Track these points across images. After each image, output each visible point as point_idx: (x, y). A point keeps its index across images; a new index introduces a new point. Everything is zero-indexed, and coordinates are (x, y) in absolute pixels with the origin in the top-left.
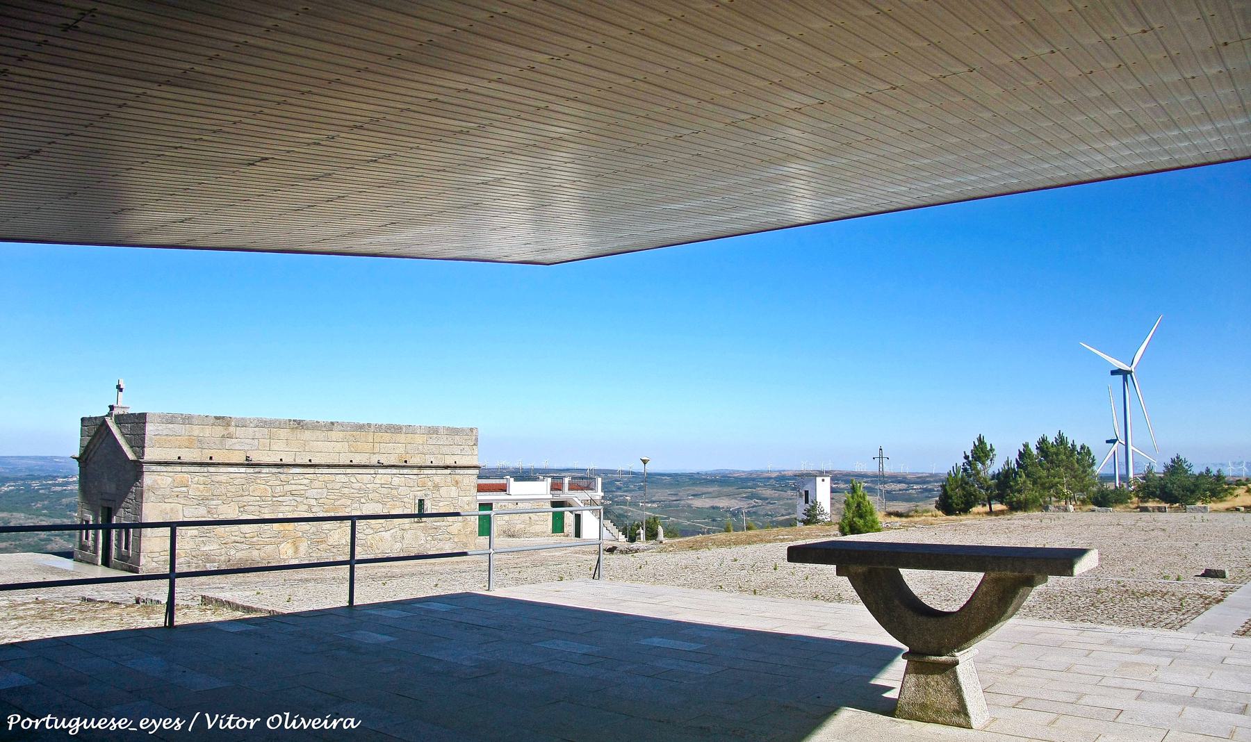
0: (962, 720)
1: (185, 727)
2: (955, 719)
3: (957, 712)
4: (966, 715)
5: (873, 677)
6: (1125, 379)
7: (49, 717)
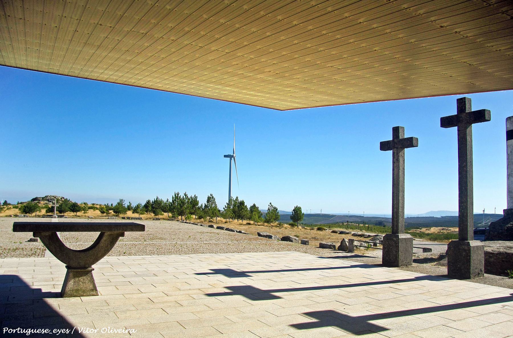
0: (94, 293)
1: (70, 332)
2: (92, 293)
3: (92, 290)
4: (96, 290)
5: (448, 259)
6: (231, 160)
7: (19, 329)
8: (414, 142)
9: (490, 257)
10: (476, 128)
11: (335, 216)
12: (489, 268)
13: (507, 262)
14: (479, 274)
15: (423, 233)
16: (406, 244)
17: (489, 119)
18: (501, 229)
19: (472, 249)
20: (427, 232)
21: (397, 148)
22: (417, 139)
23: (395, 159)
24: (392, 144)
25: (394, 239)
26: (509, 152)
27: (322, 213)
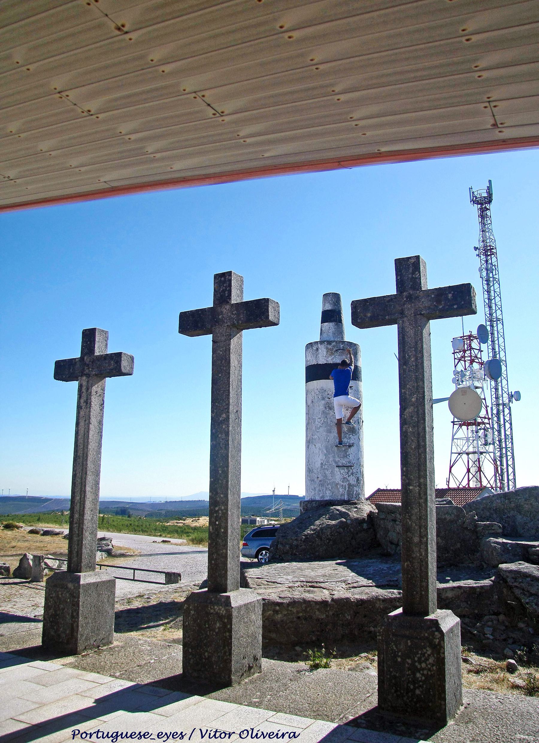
8: (124, 363)
9: (276, 612)
10: (250, 339)
11: (51, 499)
12: (273, 635)
13: (306, 619)
14: (250, 668)
15: (188, 526)
16: (99, 595)
17: (275, 321)
18: (296, 540)
19: (235, 613)
20: (194, 524)
21: (88, 376)
22: (132, 358)
23: (82, 401)
24: (78, 365)
25: (70, 585)
26: (309, 402)
27: (29, 495)
